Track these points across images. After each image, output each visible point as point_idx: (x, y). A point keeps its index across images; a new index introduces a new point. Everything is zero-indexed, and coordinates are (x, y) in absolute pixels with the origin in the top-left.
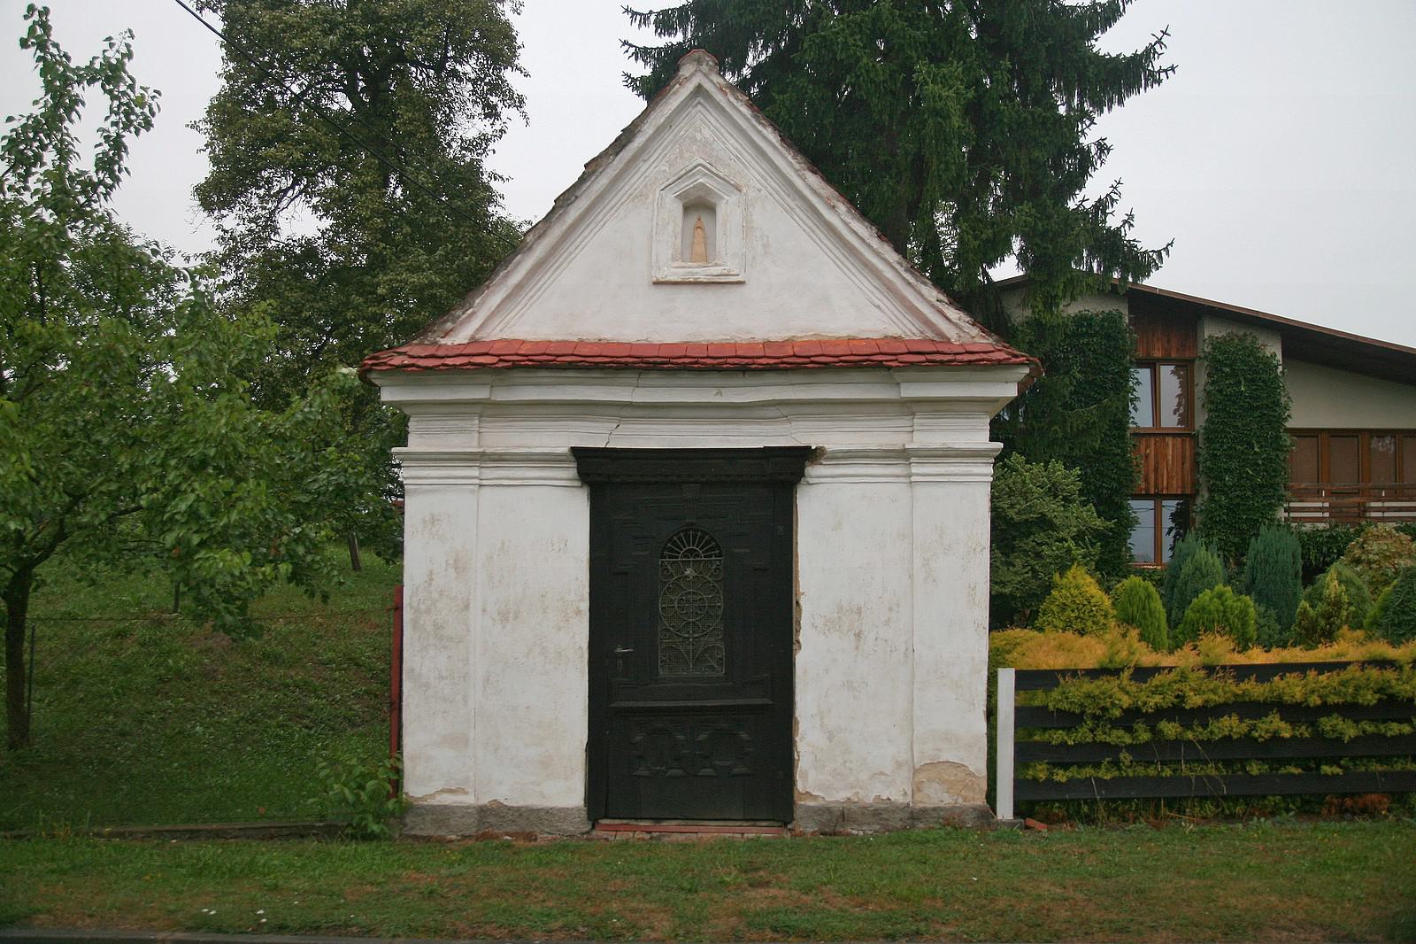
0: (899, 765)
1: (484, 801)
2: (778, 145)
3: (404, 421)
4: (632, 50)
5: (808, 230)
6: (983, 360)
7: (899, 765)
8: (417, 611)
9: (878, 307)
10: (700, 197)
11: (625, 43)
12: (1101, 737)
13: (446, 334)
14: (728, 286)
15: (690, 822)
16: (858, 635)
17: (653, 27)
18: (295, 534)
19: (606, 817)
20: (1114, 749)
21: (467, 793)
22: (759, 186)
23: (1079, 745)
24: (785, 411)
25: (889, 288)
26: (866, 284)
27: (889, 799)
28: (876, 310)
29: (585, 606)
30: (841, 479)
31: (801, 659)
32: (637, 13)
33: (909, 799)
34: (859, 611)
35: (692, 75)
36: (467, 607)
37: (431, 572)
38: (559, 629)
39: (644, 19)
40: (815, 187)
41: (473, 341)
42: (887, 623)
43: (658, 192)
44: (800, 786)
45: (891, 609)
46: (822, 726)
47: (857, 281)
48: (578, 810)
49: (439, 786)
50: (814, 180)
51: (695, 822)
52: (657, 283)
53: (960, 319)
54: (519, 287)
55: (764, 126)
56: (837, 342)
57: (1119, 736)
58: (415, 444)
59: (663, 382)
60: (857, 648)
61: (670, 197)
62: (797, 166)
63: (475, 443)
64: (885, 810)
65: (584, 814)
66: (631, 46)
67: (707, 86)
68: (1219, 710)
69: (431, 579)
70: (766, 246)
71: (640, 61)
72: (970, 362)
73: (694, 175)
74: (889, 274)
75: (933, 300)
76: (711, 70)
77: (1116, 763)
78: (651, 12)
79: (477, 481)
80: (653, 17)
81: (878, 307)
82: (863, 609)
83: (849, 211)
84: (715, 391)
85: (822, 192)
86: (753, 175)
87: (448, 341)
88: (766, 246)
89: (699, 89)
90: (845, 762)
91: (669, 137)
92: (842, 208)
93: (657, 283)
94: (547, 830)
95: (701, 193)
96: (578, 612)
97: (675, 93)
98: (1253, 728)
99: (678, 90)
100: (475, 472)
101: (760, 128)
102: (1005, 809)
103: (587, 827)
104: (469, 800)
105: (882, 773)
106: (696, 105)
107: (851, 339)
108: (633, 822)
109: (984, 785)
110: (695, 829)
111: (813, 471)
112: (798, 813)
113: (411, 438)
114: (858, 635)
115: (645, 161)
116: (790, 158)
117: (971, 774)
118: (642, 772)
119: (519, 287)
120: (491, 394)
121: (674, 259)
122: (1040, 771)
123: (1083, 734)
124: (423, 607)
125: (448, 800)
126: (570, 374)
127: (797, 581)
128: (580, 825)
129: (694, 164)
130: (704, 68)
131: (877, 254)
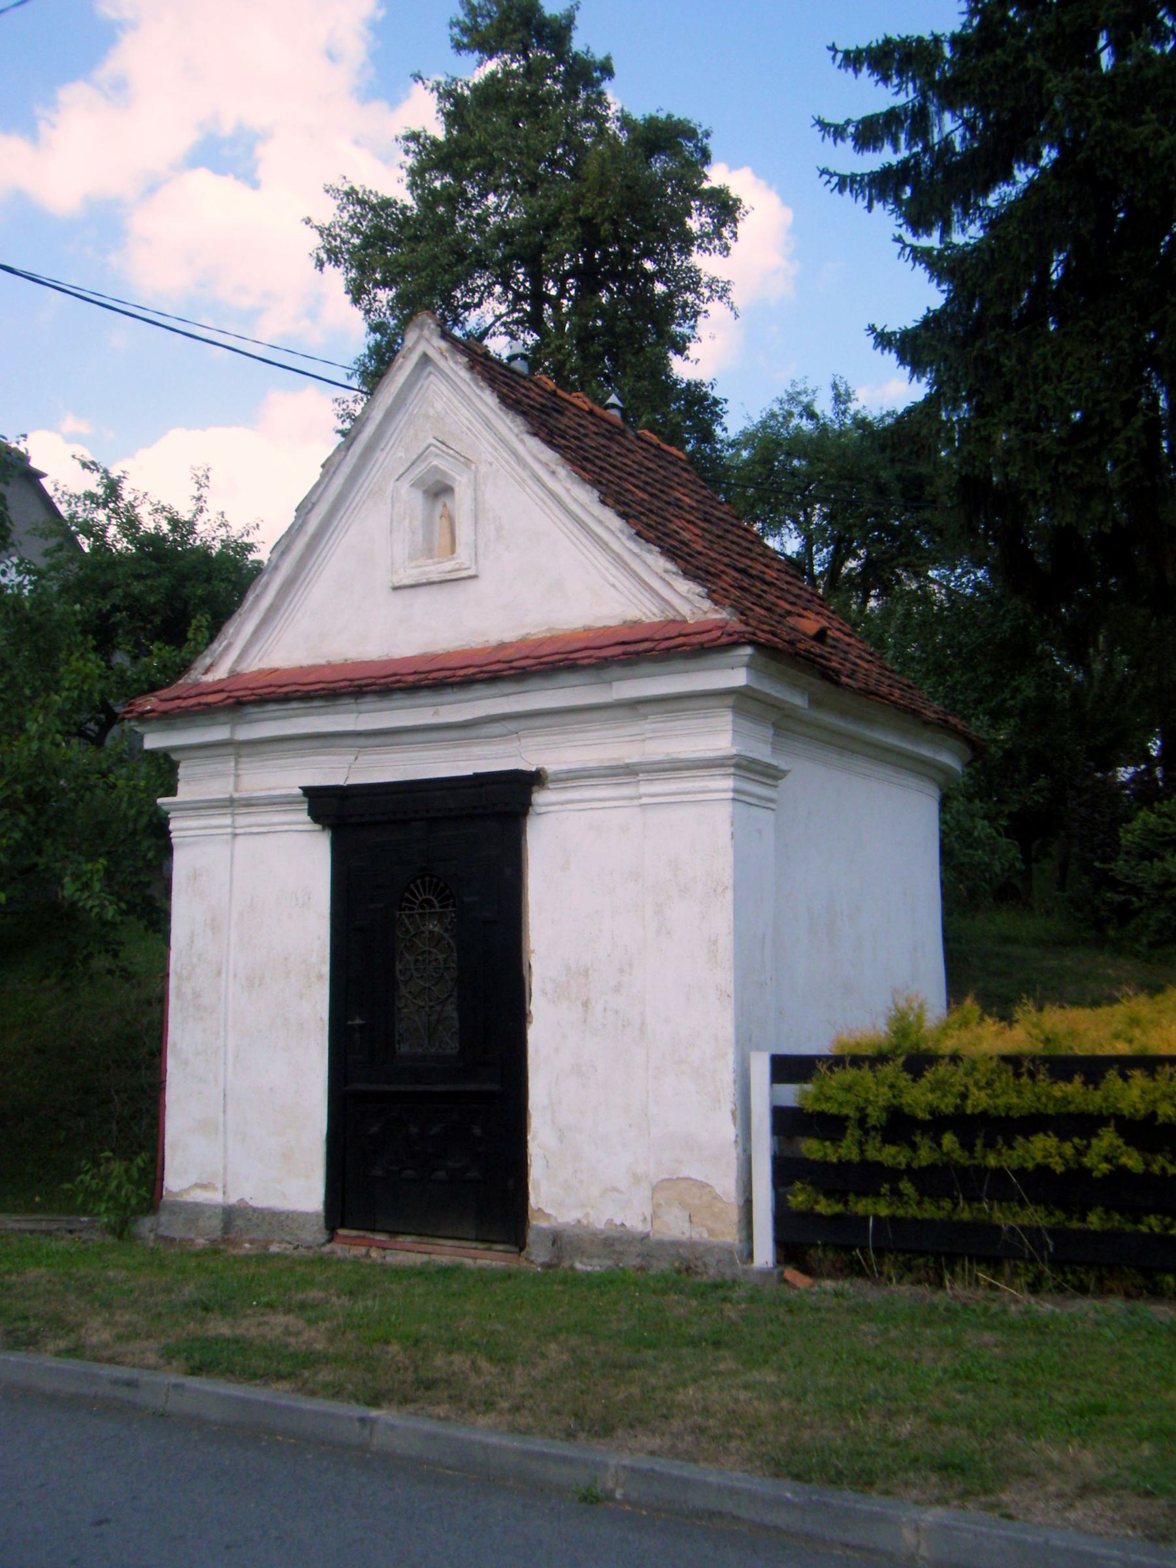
0: (637, 1179)
1: (233, 1200)
2: (496, 409)
3: (174, 767)
4: (835, 180)
5: (540, 503)
6: (684, 645)
7: (637, 1179)
8: (180, 978)
9: (613, 586)
10: (437, 482)
11: (824, 172)
12: (872, 1154)
13: (207, 671)
14: (462, 583)
15: (426, 1239)
16: (585, 1004)
17: (850, 143)
18: (101, 890)
19: (343, 1226)
20: (893, 1174)
21: (216, 1189)
22: (490, 459)
23: (844, 1166)
24: (511, 726)
25: (618, 559)
26: (601, 560)
27: (623, 1225)
28: (613, 590)
29: (326, 969)
30: (569, 806)
31: (534, 1034)
32: (829, 125)
33: (647, 1228)
34: (586, 973)
35: (417, 342)
36: (219, 973)
37: (192, 933)
38: (301, 997)
39: (837, 132)
40: (535, 452)
41: (234, 675)
42: (617, 989)
43: (392, 484)
44: (534, 1201)
45: (621, 971)
46: (553, 1122)
47: (592, 559)
48: (317, 1214)
49: (192, 1179)
50: (535, 444)
51: (430, 1240)
52: (396, 589)
53: (688, 591)
54: (273, 610)
55: (481, 388)
56: (573, 635)
57: (890, 1155)
58: (186, 792)
59: (408, 702)
60: (585, 1022)
61: (405, 486)
62: (516, 430)
63: (231, 787)
64: (619, 1239)
65: (322, 1221)
66: (832, 175)
67: (432, 353)
68: (1033, 1123)
69: (192, 942)
70: (499, 529)
71: (847, 192)
72: (668, 649)
73: (426, 458)
74: (616, 546)
75: (660, 571)
76: (432, 334)
77: (897, 1193)
78: (848, 122)
79: (229, 830)
80: (851, 129)
81: (613, 586)
82: (591, 971)
83: (569, 476)
84: (431, 710)
85: (541, 457)
86: (484, 448)
87: (209, 678)
88: (499, 529)
89: (425, 359)
90: (575, 1171)
91: (402, 418)
92: (562, 472)
93: (396, 589)
94: (288, 1238)
95: (438, 477)
96: (320, 977)
97: (400, 368)
98: (1080, 1152)
99: (402, 364)
100: (227, 820)
101: (479, 392)
102: (764, 1253)
103: (323, 1236)
104: (215, 1197)
105: (615, 1189)
106: (428, 376)
107: (587, 630)
108: (369, 1235)
109: (734, 1215)
110: (429, 1248)
111: (540, 798)
112: (531, 1236)
113: (181, 787)
114: (585, 1004)
115: (382, 450)
116: (508, 421)
117: (716, 1198)
118: (378, 1172)
119: (273, 610)
120: (233, 732)
121: (412, 558)
122: (798, 1199)
123: (847, 1150)
124: (185, 973)
125: (199, 1196)
126: (294, 705)
127: (526, 850)
128: (315, 1233)
129: (425, 445)
130: (426, 333)
131: (601, 522)
